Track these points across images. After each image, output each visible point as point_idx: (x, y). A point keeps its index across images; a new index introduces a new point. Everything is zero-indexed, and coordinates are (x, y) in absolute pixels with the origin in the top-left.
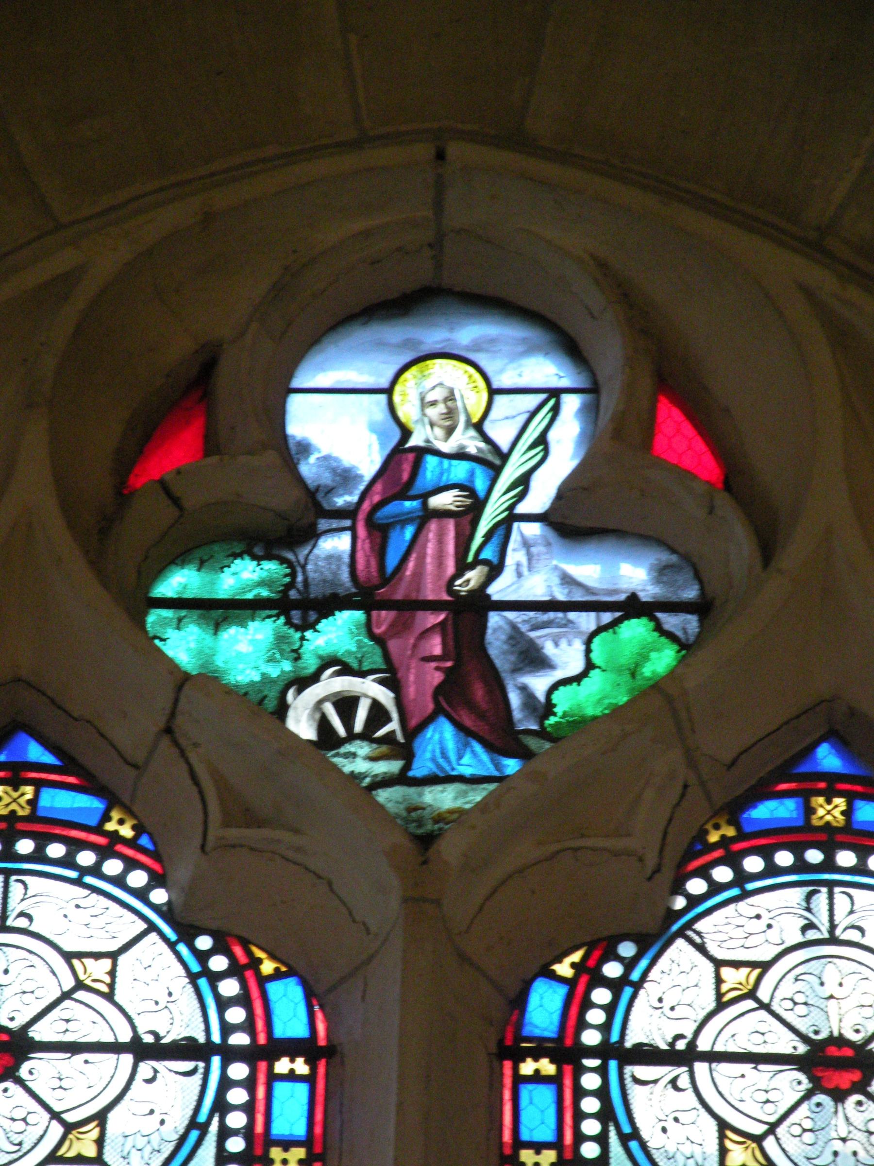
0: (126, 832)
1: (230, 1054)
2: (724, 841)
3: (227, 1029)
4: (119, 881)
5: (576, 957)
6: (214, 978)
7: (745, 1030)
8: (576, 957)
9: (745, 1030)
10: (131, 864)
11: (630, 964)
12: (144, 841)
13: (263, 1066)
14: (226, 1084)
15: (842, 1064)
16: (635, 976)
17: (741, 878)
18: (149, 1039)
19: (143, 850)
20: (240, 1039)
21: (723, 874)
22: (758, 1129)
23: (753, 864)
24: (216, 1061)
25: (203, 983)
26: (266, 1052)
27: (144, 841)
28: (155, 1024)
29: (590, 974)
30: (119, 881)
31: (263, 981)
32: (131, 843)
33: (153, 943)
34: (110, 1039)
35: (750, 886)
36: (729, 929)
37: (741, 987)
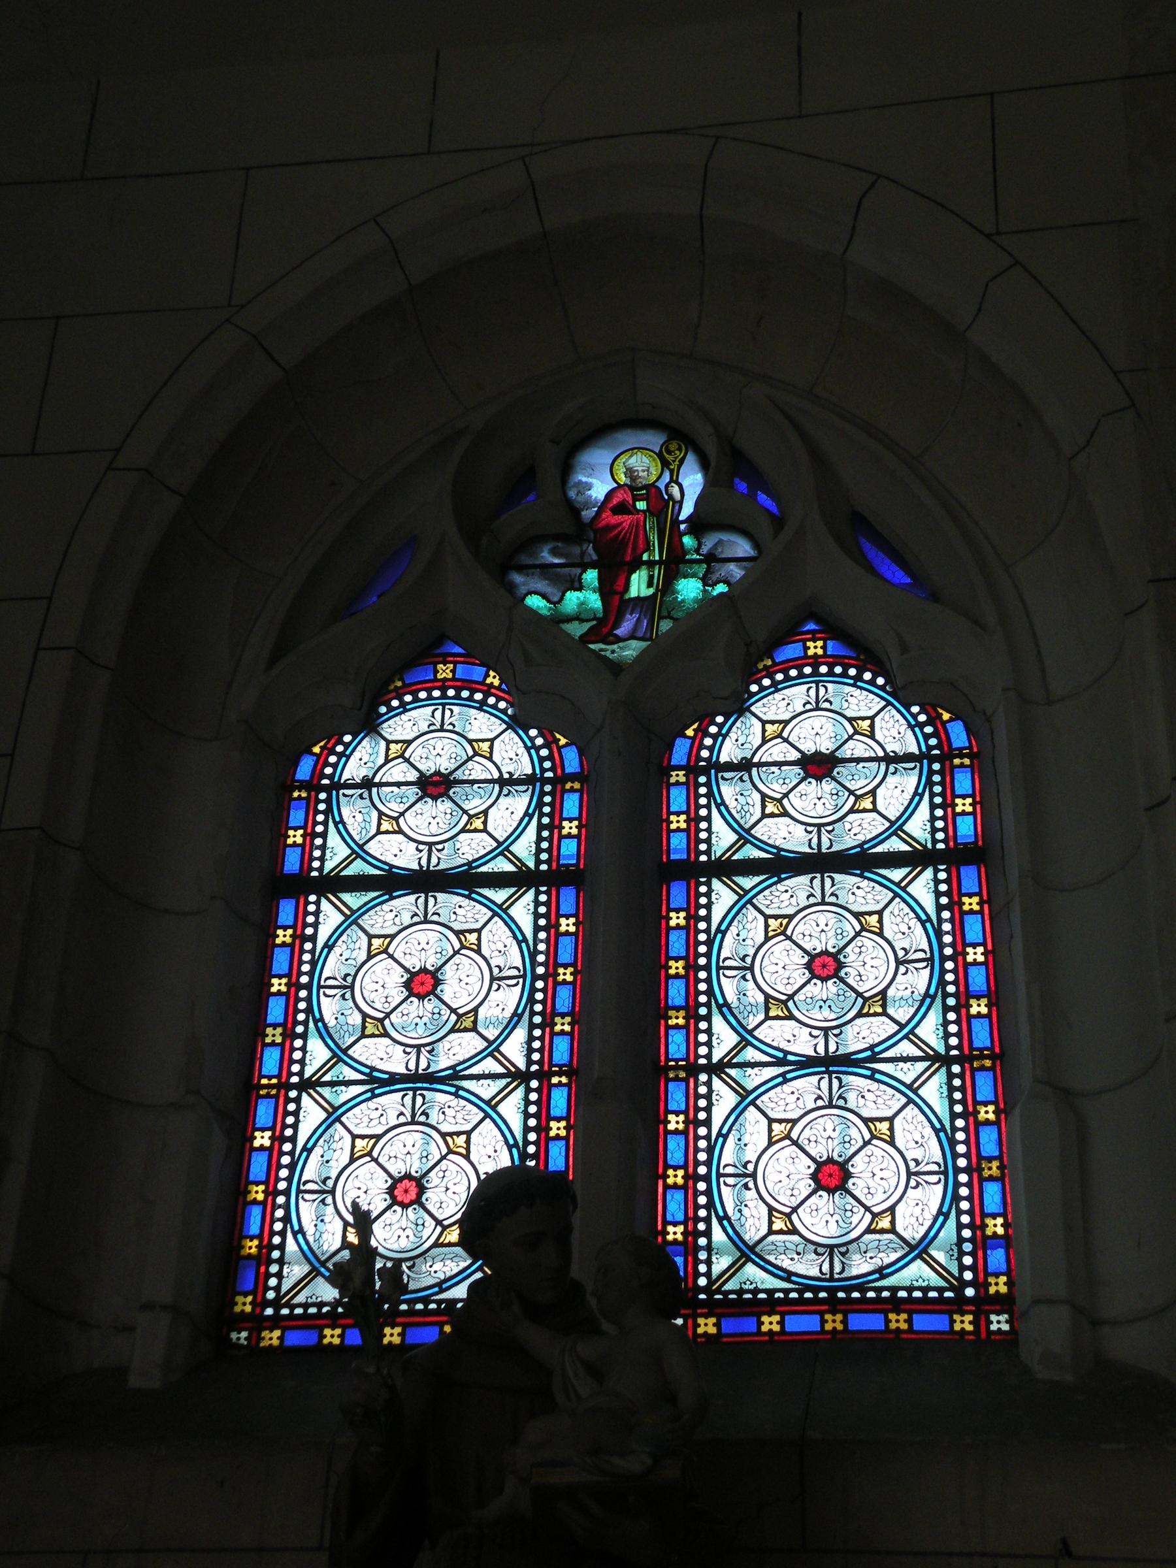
0: (496, 682)
1: (932, 759)
2: (491, 685)
3: (543, 770)
4: (495, 707)
5: (695, 726)
6: (538, 749)
7: (777, 751)
8: (695, 726)
9: (777, 751)
10: (499, 699)
11: (721, 726)
12: (504, 686)
13: (948, 763)
14: (931, 772)
15: (436, 784)
16: (724, 731)
17: (403, 704)
18: (506, 776)
19: (503, 691)
20: (549, 774)
21: (766, 682)
22: (779, 796)
23: (779, 677)
24: (538, 784)
25: (533, 751)
26: (560, 780)
27: (504, 686)
28: (893, 747)
29: (703, 732)
30: (495, 707)
31: (944, 723)
32: (499, 688)
33: (510, 734)
34: (490, 777)
35: (859, 684)
36: (773, 707)
37: (779, 730)
